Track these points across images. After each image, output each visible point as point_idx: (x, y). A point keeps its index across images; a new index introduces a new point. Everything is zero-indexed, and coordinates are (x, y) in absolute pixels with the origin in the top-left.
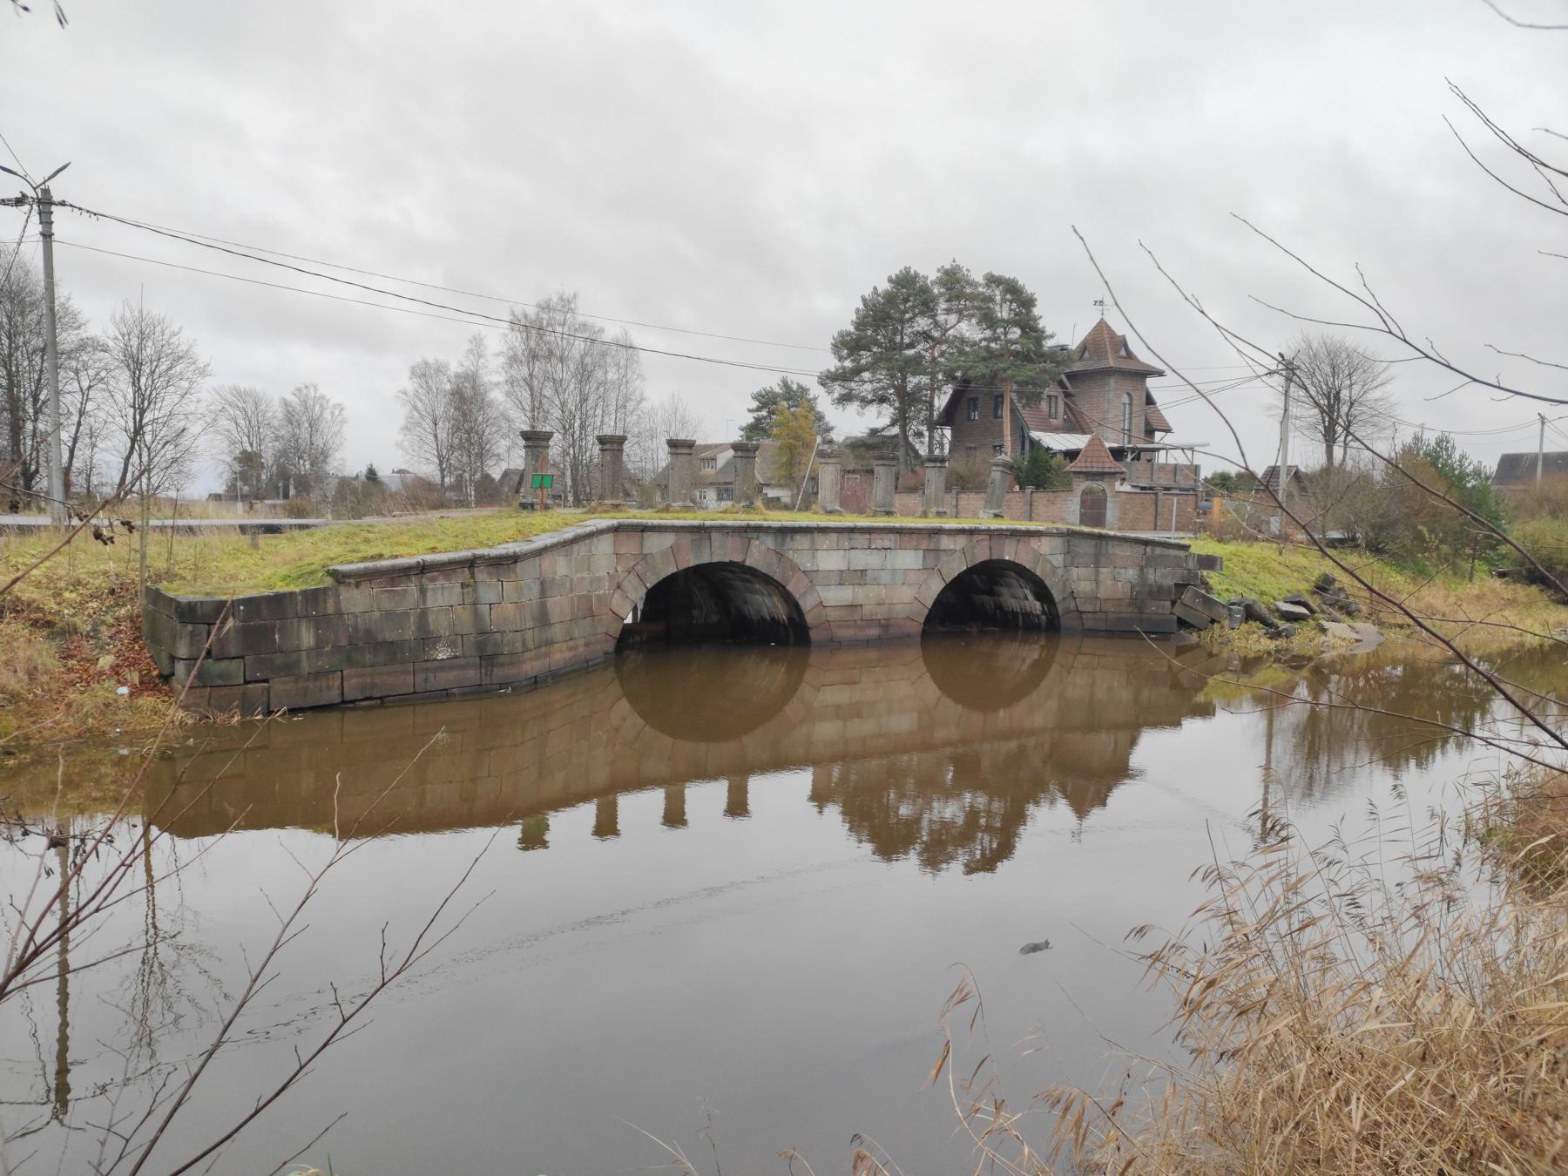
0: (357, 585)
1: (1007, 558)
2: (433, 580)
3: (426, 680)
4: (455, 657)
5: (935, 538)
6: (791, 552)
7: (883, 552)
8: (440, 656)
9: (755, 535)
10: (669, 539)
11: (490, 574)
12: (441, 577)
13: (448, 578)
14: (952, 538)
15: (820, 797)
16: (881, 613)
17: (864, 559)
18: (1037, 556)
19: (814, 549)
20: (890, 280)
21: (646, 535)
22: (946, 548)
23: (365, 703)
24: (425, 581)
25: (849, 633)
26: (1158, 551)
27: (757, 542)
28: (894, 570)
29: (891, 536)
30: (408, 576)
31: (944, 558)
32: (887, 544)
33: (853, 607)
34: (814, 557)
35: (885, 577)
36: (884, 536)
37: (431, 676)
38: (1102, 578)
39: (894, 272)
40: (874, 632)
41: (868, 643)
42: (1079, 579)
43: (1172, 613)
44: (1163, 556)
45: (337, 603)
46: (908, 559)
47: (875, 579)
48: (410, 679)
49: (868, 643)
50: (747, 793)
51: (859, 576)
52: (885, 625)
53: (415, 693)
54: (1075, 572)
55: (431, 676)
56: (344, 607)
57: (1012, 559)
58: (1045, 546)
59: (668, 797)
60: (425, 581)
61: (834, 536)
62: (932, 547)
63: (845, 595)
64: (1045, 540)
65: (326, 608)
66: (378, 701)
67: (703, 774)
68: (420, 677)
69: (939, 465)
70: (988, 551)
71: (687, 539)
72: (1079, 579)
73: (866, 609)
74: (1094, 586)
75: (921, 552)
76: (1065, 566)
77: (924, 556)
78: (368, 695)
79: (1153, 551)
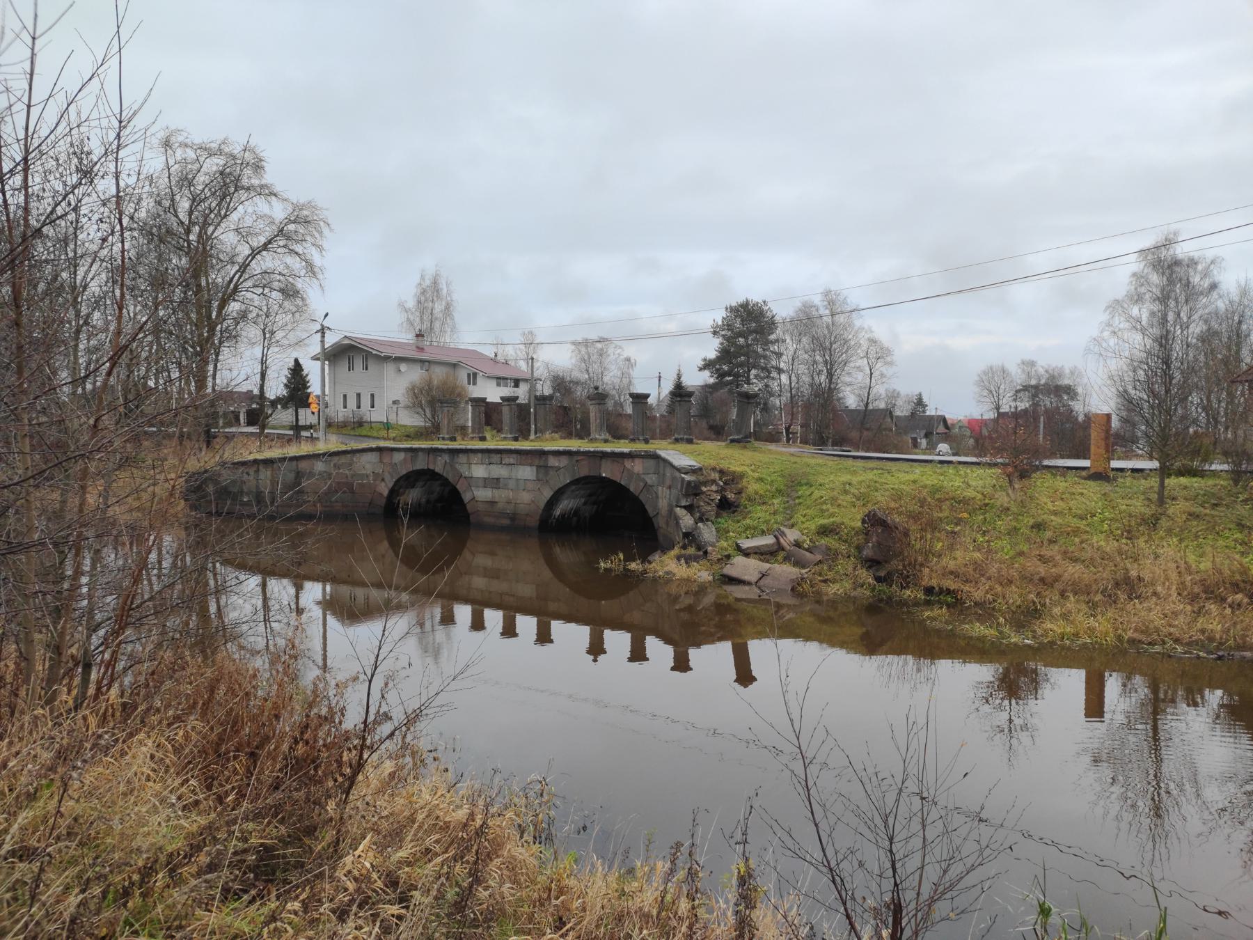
17: (499, 471)
18: (631, 474)
29: (514, 456)
31: (552, 473)
32: (512, 461)
33: (492, 503)
35: (512, 484)
40: (506, 522)
46: (526, 472)
52: (513, 517)
58: (637, 466)
61: (480, 455)
62: (542, 464)
64: (637, 461)
73: (500, 505)
75: (534, 468)
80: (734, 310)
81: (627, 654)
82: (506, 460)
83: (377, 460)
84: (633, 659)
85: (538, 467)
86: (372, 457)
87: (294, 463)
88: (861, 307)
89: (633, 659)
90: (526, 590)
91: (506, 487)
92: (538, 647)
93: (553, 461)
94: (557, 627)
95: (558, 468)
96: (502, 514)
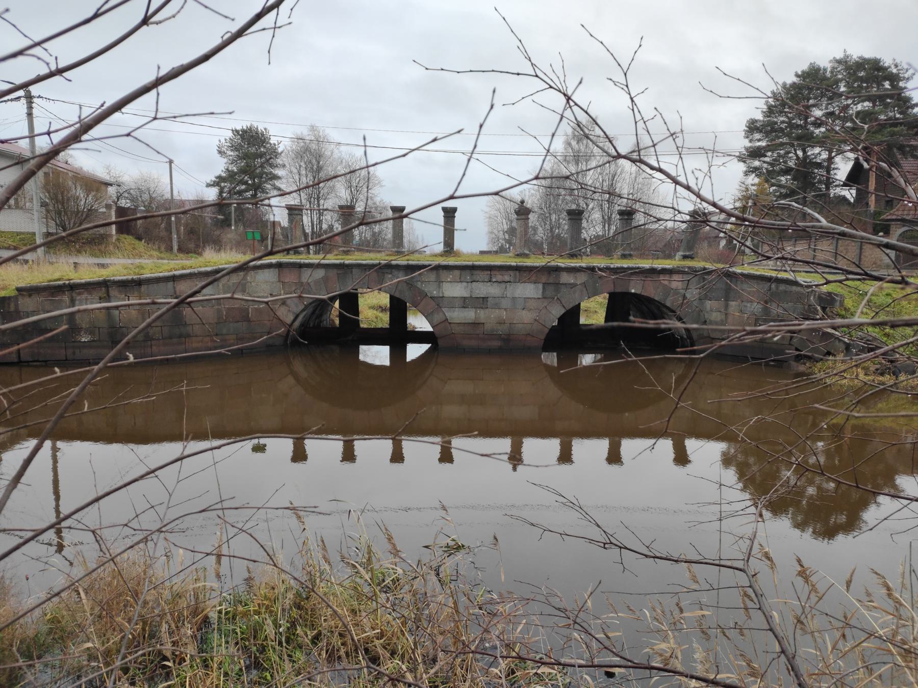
0: (30, 296)
1: (633, 291)
2: (79, 294)
3: (74, 353)
4: (94, 341)
5: (554, 275)
6: (419, 283)
7: (503, 285)
8: (83, 340)
9: (389, 271)
10: (320, 273)
11: (120, 292)
12: (86, 293)
13: (90, 293)
14: (572, 275)
15: (727, 461)
16: (502, 330)
17: (483, 289)
18: (667, 291)
19: (439, 282)
20: (797, 75)
21: (303, 270)
22: (565, 282)
23: (35, 363)
24: (74, 295)
25: (473, 343)
26: (782, 287)
27: (390, 276)
28: (514, 299)
29: (511, 273)
30: (64, 292)
31: (564, 290)
32: (507, 278)
33: (475, 324)
34: (439, 287)
35: (505, 303)
36: (503, 272)
37: (77, 351)
38: (731, 310)
39: (804, 67)
40: (496, 344)
41: (490, 352)
42: (711, 311)
43: (790, 344)
44: (786, 292)
45: (17, 305)
46: (529, 290)
47: (496, 304)
48: (63, 351)
49: (490, 352)
50: (402, 448)
51: (482, 302)
52: (507, 339)
53: (66, 360)
54: (708, 304)
55: (77, 351)
56: (21, 308)
57: (638, 292)
58: (676, 283)
59: (562, 444)
60: (74, 295)
61: (457, 272)
62: (551, 281)
63: (469, 315)
64: (676, 277)
65: (9, 307)
66: (43, 364)
67: (325, 431)
68: (70, 352)
69: (626, 217)
70: (612, 286)
71: (333, 273)
72: (711, 311)
73: (488, 327)
74: (723, 317)
75: (540, 286)
76: (700, 299)
77: (544, 288)
78: (36, 359)
79: (777, 288)
80: (217, 178)
81: (290, 454)
82: (499, 277)
83: (275, 279)
84: (441, 460)
85: (545, 285)
86: (269, 276)
87: (170, 284)
88: (614, 142)
89: (441, 460)
90: (525, 413)
91: (497, 306)
92: (267, 452)
93: (566, 278)
94: (692, 445)
95: (573, 286)
96: (492, 336)
